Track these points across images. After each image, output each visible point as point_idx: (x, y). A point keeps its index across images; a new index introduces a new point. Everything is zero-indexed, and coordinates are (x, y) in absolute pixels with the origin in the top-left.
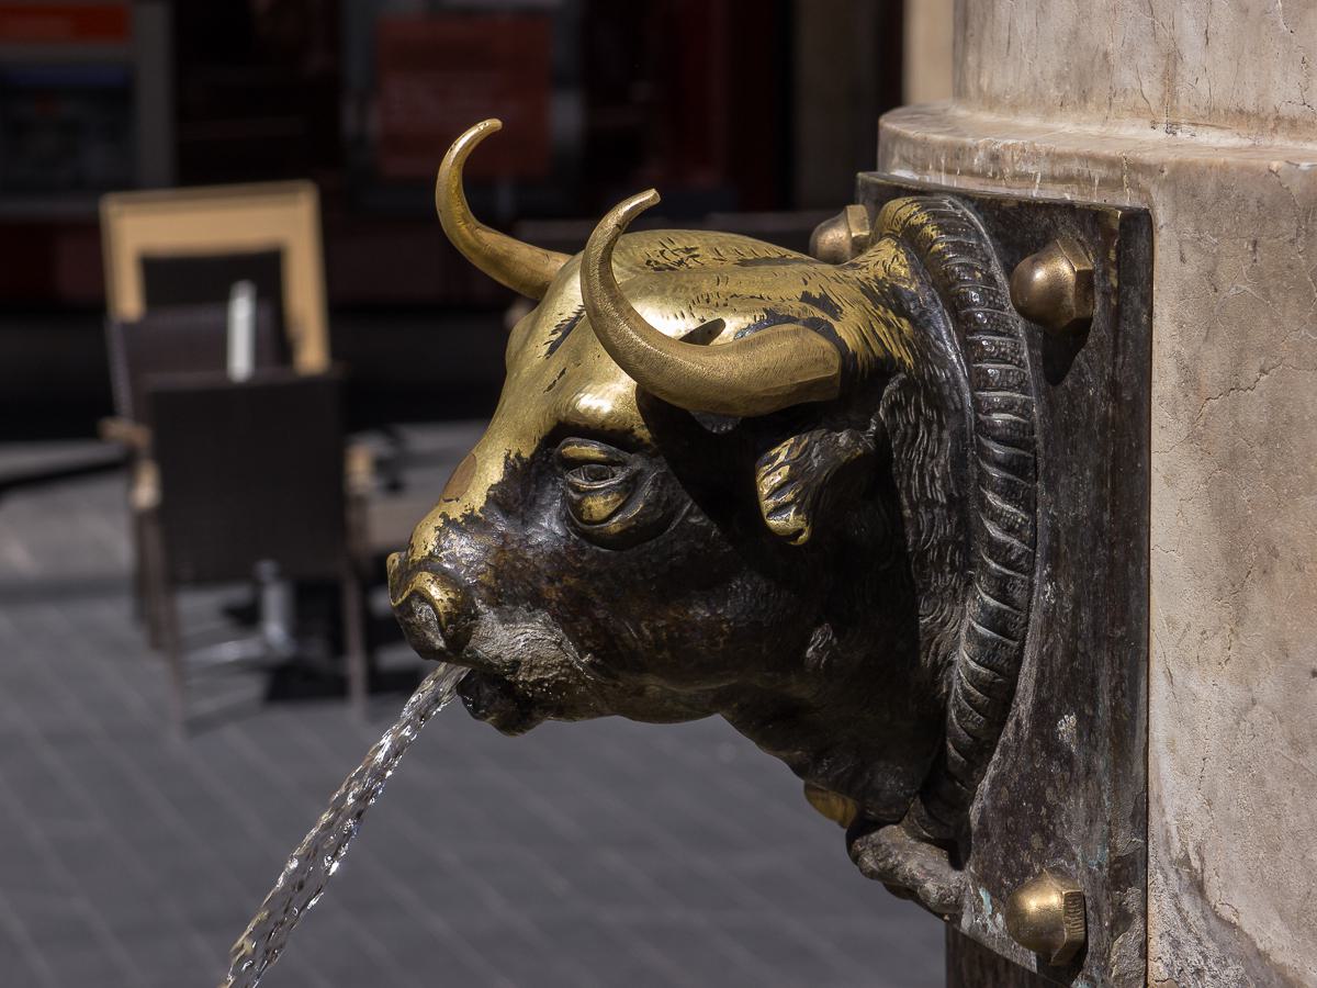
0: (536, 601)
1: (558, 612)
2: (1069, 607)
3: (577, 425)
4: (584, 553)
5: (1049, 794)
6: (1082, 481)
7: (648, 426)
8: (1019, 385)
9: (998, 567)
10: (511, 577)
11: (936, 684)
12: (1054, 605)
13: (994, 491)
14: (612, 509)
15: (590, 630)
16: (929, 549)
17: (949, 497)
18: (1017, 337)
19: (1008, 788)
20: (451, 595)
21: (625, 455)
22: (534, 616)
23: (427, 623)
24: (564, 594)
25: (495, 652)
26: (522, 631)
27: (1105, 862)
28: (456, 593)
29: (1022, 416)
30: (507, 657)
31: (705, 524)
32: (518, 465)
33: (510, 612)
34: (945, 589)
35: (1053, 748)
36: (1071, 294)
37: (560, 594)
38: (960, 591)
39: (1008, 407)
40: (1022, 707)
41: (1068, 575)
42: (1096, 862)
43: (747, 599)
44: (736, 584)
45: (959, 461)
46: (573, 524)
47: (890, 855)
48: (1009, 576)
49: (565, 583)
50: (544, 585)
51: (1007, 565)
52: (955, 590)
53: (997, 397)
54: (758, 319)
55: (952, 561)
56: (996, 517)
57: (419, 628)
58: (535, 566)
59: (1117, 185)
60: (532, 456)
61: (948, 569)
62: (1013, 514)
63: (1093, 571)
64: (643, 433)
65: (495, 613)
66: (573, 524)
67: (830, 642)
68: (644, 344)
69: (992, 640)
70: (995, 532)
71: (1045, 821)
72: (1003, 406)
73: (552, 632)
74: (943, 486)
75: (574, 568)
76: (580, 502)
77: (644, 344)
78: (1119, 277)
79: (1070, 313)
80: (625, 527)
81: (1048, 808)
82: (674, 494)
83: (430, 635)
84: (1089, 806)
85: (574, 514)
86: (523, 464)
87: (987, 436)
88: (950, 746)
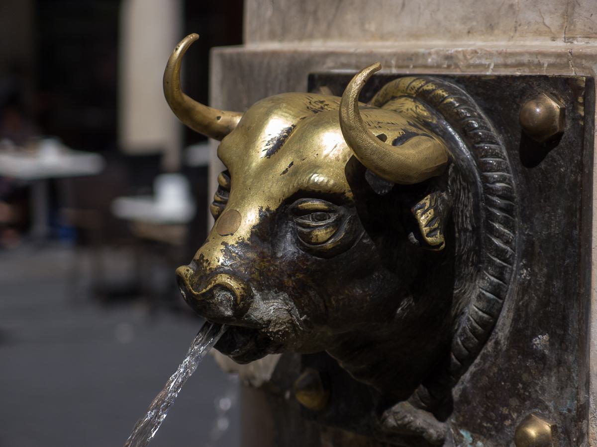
0: (281, 287)
1: (292, 293)
2: (542, 280)
3: (314, 191)
4: (308, 260)
5: (525, 377)
6: (555, 216)
7: (352, 191)
8: (506, 169)
9: (500, 262)
10: (268, 275)
11: (453, 324)
12: (529, 281)
13: (499, 223)
14: (330, 236)
15: (308, 302)
16: (463, 254)
17: (473, 226)
18: (500, 145)
19: (487, 376)
20: (242, 286)
21: (336, 207)
22: (278, 296)
23: (221, 302)
24: (296, 283)
25: (260, 316)
26: (272, 304)
27: (575, 407)
28: (244, 285)
29: (509, 184)
30: (265, 318)
31: (370, 243)
32: (268, 215)
33: (267, 294)
34: (469, 274)
35: (530, 353)
36: (557, 120)
37: (294, 283)
38: (474, 275)
39: (503, 180)
40: (500, 334)
41: (542, 264)
42: (566, 409)
43: (380, 283)
44: (376, 275)
45: (476, 208)
46: (301, 244)
47: (405, 417)
48: (505, 266)
49: (297, 277)
50: (286, 279)
51: (505, 261)
52: (472, 275)
53: (496, 175)
54: (401, 134)
55: (473, 260)
56: (500, 236)
57: (216, 305)
58: (281, 268)
59: (566, 66)
60: (277, 210)
61: (470, 264)
62: (509, 234)
63: (564, 260)
64: (349, 195)
65: (260, 295)
66: (301, 244)
67: (410, 305)
68: (375, 144)
69: (493, 299)
70: (497, 242)
71: (522, 391)
72: (501, 179)
73: (287, 304)
74: (470, 221)
75: (302, 268)
76: (310, 233)
77: (375, 144)
78: (584, 110)
79: (555, 129)
80: (335, 245)
81: (524, 384)
82: (358, 227)
83: (222, 309)
84: (560, 380)
85: (304, 240)
86: (271, 214)
87: (493, 195)
88: (453, 357)
